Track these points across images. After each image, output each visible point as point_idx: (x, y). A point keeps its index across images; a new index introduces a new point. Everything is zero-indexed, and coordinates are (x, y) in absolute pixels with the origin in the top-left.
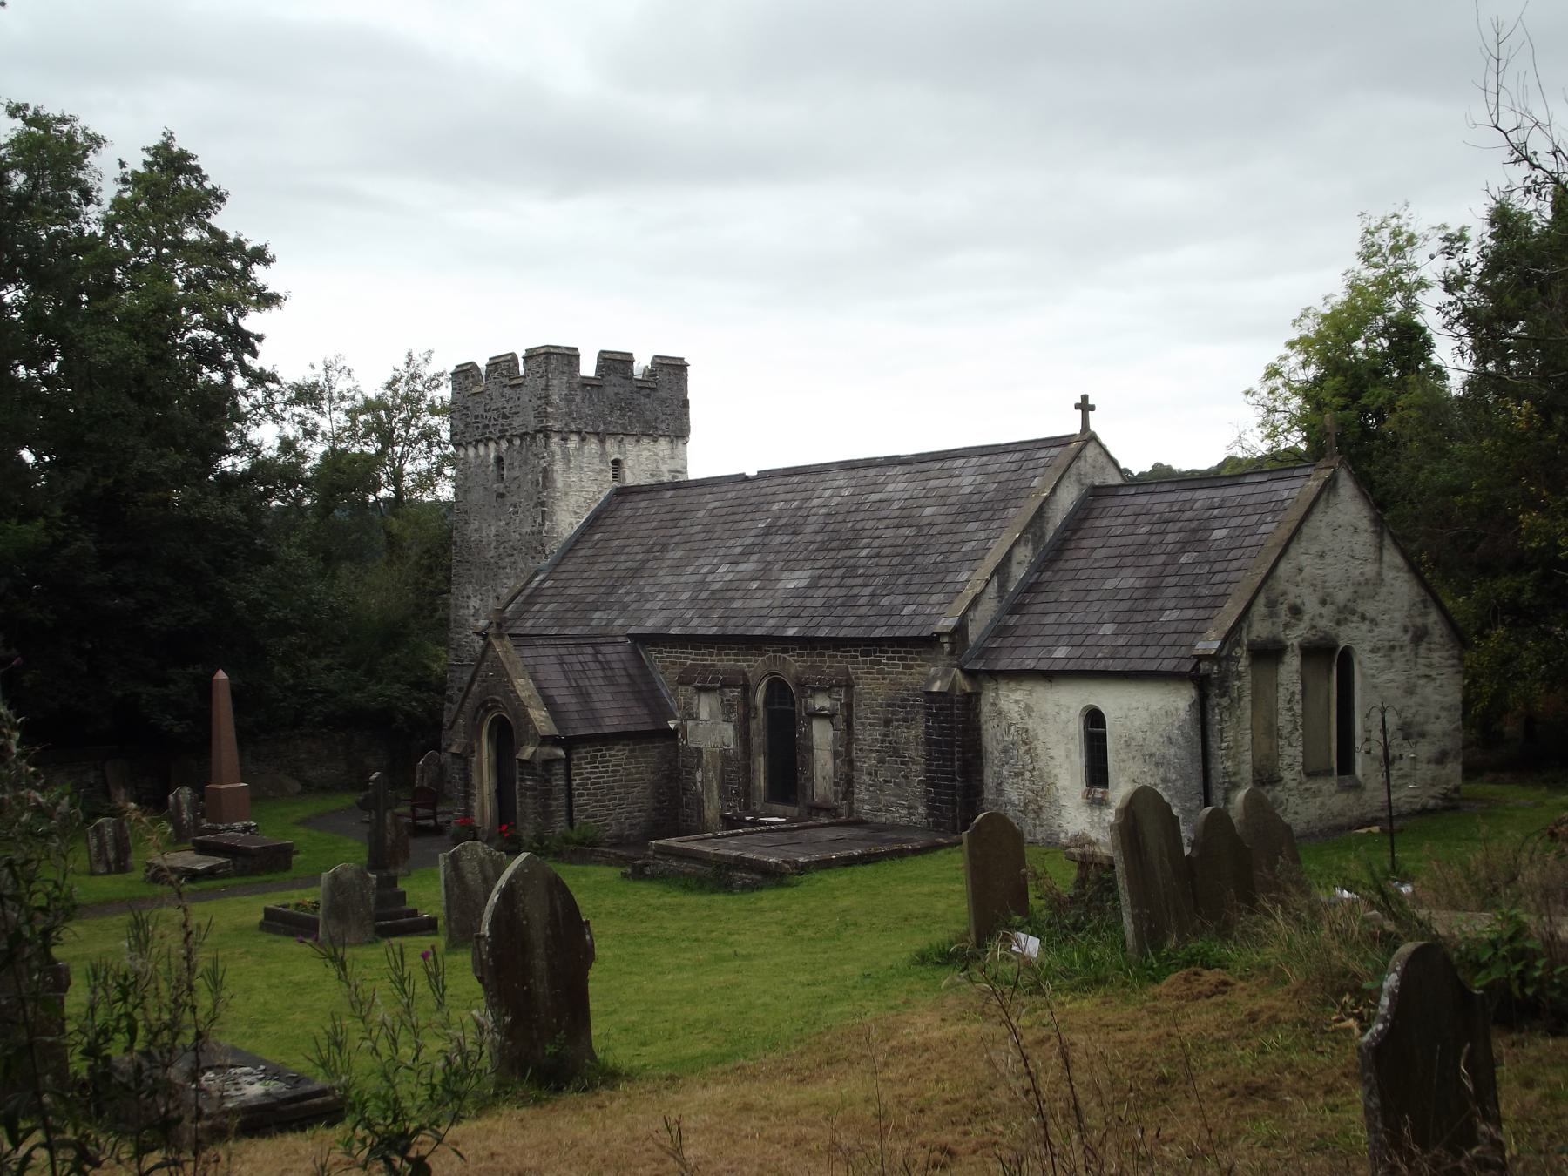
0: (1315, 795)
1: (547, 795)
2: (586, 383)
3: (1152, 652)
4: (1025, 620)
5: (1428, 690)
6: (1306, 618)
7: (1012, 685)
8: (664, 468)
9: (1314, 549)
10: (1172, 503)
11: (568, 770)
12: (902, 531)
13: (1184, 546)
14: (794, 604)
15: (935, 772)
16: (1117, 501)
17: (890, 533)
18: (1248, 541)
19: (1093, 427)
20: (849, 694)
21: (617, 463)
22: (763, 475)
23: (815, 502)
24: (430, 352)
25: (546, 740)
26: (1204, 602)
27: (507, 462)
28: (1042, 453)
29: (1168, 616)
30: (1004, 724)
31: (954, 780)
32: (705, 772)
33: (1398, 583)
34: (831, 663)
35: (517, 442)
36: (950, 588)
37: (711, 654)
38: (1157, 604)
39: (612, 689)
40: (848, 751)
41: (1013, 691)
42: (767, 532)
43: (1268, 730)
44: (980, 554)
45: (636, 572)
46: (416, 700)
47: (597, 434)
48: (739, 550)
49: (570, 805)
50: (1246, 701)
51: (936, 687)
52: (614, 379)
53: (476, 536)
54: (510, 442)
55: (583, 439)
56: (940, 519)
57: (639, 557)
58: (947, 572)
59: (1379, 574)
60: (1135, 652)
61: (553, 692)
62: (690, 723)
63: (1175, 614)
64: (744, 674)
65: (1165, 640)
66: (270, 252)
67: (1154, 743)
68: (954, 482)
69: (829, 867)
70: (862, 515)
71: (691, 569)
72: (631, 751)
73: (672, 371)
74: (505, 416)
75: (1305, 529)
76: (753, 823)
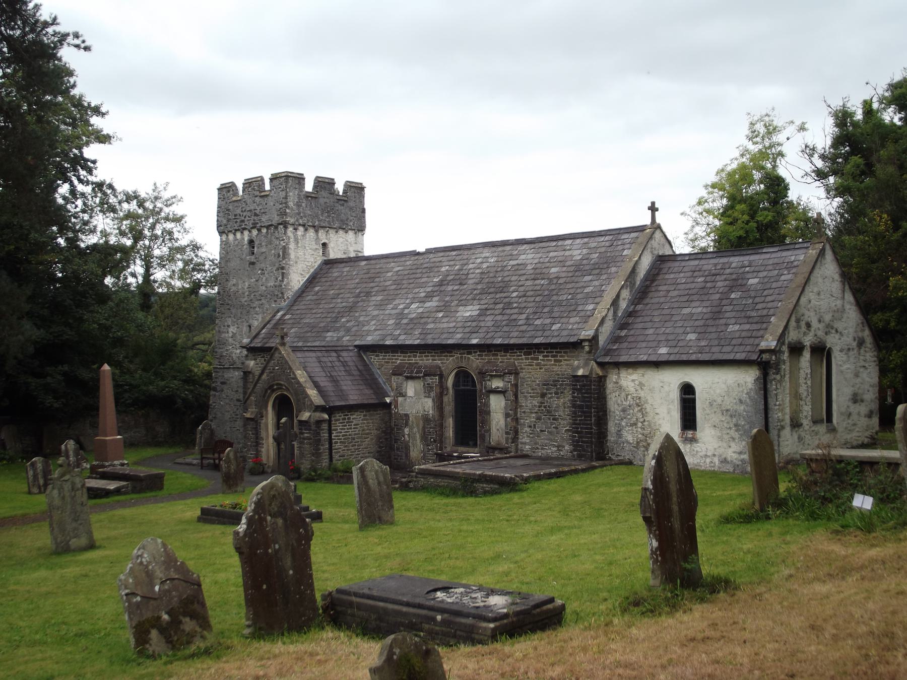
0: (817, 434)
1: (317, 442)
2: (308, 196)
3: (727, 349)
4: (632, 332)
5: (864, 375)
6: (813, 329)
7: (630, 371)
8: (351, 249)
9: (816, 290)
10: (715, 265)
11: (330, 426)
12: (537, 282)
13: (731, 289)
14: (474, 324)
15: (579, 424)
16: (677, 264)
17: (529, 283)
18: (774, 285)
19: (658, 221)
20: (516, 379)
21: (324, 245)
22: (429, 251)
23: (471, 266)
24: (167, 184)
25: (318, 409)
26: (755, 320)
27: (256, 243)
28: (626, 236)
29: (731, 328)
30: (623, 394)
31: (591, 428)
32: (411, 429)
33: (851, 312)
34: (503, 360)
35: (264, 231)
36: (582, 314)
37: (415, 356)
38: (723, 321)
39: (351, 378)
40: (516, 414)
41: (630, 374)
42: (441, 284)
43: (796, 396)
44: (598, 294)
45: (351, 309)
46: (187, 390)
47: (314, 227)
48: (423, 295)
49: (330, 449)
50: (787, 378)
51: (580, 372)
52: (324, 193)
53: (234, 288)
54: (259, 230)
55: (306, 230)
56: (563, 275)
57: (351, 300)
58: (577, 305)
59: (843, 306)
60: (714, 349)
61: (318, 379)
62: (400, 399)
63: (737, 327)
64: (440, 368)
65: (734, 342)
66: (103, 110)
67: (729, 403)
68: (567, 253)
69: (540, 480)
70: (506, 273)
71: (391, 306)
72: (365, 416)
73: (356, 190)
74: (256, 215)
75: (812, 278)
76: (459, 457)
